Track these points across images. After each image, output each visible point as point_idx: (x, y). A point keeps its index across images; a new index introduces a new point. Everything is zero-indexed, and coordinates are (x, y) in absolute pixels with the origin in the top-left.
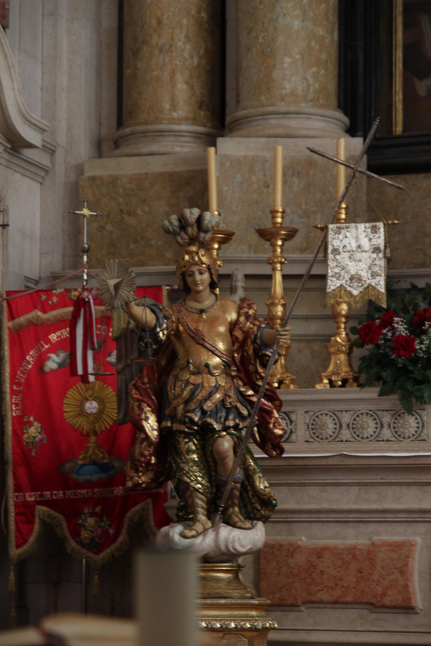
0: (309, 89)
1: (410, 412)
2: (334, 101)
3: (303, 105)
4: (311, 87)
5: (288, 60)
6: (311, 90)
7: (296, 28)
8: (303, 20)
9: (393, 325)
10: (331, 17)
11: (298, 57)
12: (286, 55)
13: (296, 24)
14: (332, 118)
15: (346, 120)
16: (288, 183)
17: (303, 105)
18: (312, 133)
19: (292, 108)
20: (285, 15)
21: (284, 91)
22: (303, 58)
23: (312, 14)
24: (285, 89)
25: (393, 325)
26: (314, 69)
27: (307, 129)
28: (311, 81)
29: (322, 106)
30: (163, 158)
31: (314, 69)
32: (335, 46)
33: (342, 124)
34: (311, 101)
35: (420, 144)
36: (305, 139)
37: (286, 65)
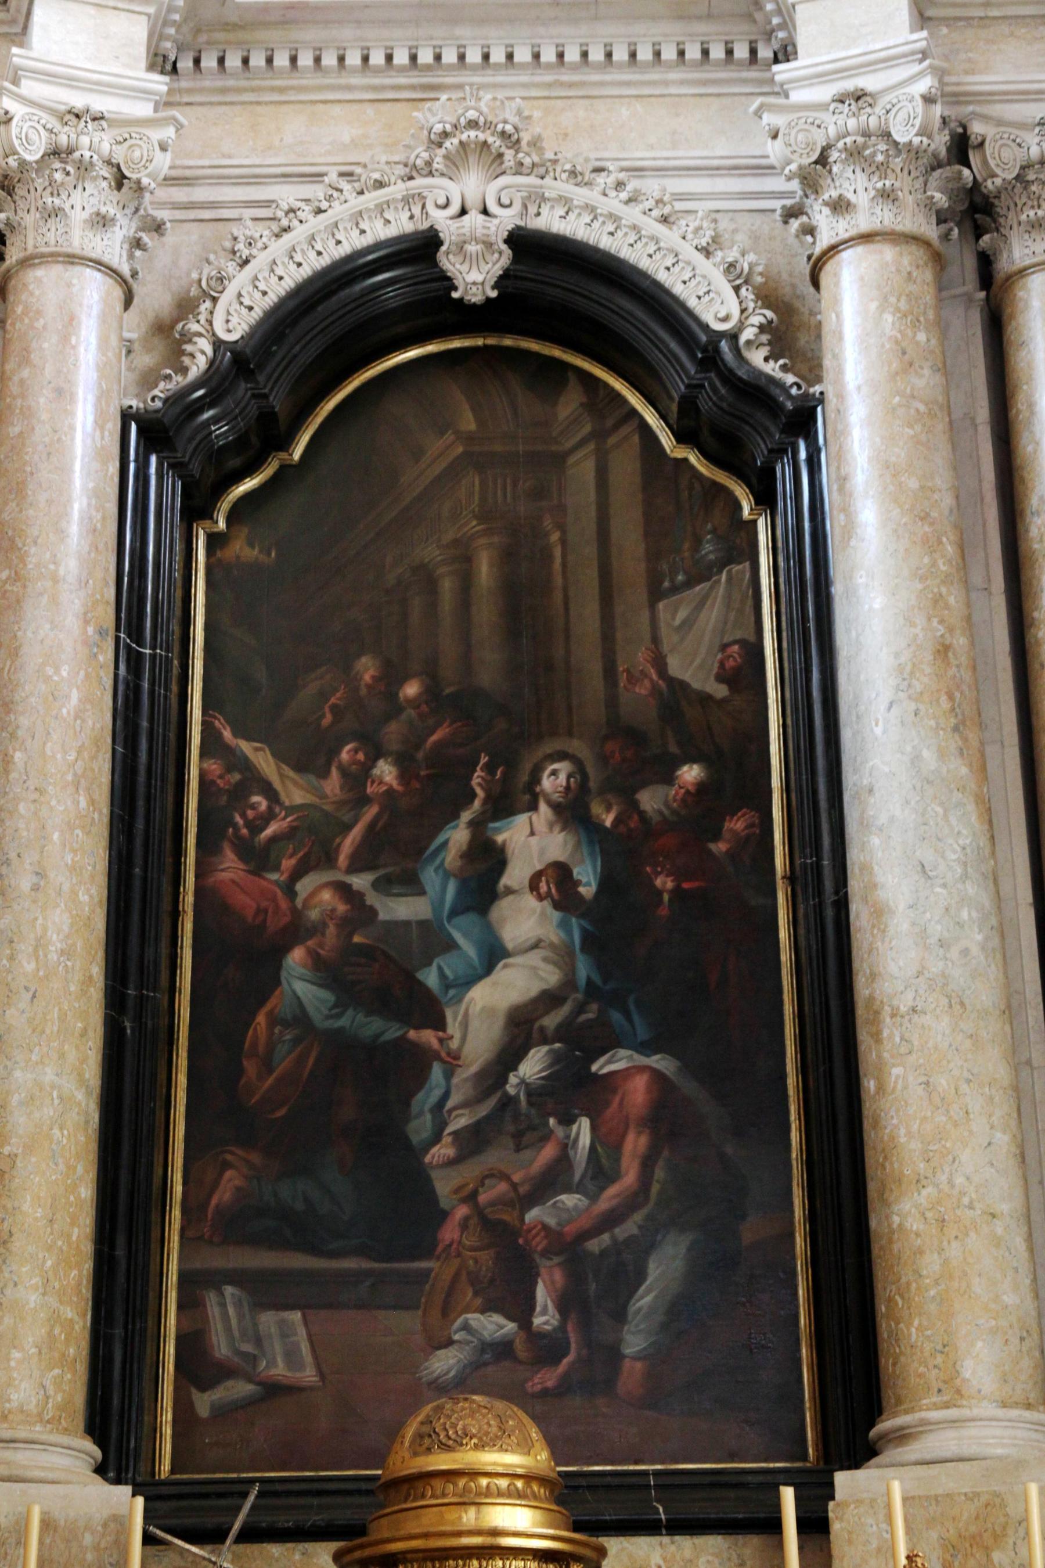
0: (47, 1403)
2: (80, 1423)
3: (38, 1428)
4: (51, 1400)
5: (16, 1355)
6: (50, 1405)
7: (32, 1305)
8: (44, 1294)
9: (395, 784)
10: (84, 1291)
11: (33, 1350)
12: (15, 1347)
13: (33, 1299)
14: (79, 1451)
15: (98, 1453)
16: (9, 1557)
17: (38, 1428)
18: (50, 1476)
19: (22, 1434)
20: (16, 1285)
21: (7, 1405)
22: (40, 1353)
23: (57, 1285)
24: (9, 1401)
25: (395, 784)
26: (57, 1371)
27: (43, 1468)
28: (51, 1392)
29: (66, 1431)
30: (983, 1463)
31: (57, 1371)
32: (86, 1335)
33: (92, 1461)
34: (48, 1422)
35: (206, 1496)
36: (40, 1485)
37: (13, 1364)
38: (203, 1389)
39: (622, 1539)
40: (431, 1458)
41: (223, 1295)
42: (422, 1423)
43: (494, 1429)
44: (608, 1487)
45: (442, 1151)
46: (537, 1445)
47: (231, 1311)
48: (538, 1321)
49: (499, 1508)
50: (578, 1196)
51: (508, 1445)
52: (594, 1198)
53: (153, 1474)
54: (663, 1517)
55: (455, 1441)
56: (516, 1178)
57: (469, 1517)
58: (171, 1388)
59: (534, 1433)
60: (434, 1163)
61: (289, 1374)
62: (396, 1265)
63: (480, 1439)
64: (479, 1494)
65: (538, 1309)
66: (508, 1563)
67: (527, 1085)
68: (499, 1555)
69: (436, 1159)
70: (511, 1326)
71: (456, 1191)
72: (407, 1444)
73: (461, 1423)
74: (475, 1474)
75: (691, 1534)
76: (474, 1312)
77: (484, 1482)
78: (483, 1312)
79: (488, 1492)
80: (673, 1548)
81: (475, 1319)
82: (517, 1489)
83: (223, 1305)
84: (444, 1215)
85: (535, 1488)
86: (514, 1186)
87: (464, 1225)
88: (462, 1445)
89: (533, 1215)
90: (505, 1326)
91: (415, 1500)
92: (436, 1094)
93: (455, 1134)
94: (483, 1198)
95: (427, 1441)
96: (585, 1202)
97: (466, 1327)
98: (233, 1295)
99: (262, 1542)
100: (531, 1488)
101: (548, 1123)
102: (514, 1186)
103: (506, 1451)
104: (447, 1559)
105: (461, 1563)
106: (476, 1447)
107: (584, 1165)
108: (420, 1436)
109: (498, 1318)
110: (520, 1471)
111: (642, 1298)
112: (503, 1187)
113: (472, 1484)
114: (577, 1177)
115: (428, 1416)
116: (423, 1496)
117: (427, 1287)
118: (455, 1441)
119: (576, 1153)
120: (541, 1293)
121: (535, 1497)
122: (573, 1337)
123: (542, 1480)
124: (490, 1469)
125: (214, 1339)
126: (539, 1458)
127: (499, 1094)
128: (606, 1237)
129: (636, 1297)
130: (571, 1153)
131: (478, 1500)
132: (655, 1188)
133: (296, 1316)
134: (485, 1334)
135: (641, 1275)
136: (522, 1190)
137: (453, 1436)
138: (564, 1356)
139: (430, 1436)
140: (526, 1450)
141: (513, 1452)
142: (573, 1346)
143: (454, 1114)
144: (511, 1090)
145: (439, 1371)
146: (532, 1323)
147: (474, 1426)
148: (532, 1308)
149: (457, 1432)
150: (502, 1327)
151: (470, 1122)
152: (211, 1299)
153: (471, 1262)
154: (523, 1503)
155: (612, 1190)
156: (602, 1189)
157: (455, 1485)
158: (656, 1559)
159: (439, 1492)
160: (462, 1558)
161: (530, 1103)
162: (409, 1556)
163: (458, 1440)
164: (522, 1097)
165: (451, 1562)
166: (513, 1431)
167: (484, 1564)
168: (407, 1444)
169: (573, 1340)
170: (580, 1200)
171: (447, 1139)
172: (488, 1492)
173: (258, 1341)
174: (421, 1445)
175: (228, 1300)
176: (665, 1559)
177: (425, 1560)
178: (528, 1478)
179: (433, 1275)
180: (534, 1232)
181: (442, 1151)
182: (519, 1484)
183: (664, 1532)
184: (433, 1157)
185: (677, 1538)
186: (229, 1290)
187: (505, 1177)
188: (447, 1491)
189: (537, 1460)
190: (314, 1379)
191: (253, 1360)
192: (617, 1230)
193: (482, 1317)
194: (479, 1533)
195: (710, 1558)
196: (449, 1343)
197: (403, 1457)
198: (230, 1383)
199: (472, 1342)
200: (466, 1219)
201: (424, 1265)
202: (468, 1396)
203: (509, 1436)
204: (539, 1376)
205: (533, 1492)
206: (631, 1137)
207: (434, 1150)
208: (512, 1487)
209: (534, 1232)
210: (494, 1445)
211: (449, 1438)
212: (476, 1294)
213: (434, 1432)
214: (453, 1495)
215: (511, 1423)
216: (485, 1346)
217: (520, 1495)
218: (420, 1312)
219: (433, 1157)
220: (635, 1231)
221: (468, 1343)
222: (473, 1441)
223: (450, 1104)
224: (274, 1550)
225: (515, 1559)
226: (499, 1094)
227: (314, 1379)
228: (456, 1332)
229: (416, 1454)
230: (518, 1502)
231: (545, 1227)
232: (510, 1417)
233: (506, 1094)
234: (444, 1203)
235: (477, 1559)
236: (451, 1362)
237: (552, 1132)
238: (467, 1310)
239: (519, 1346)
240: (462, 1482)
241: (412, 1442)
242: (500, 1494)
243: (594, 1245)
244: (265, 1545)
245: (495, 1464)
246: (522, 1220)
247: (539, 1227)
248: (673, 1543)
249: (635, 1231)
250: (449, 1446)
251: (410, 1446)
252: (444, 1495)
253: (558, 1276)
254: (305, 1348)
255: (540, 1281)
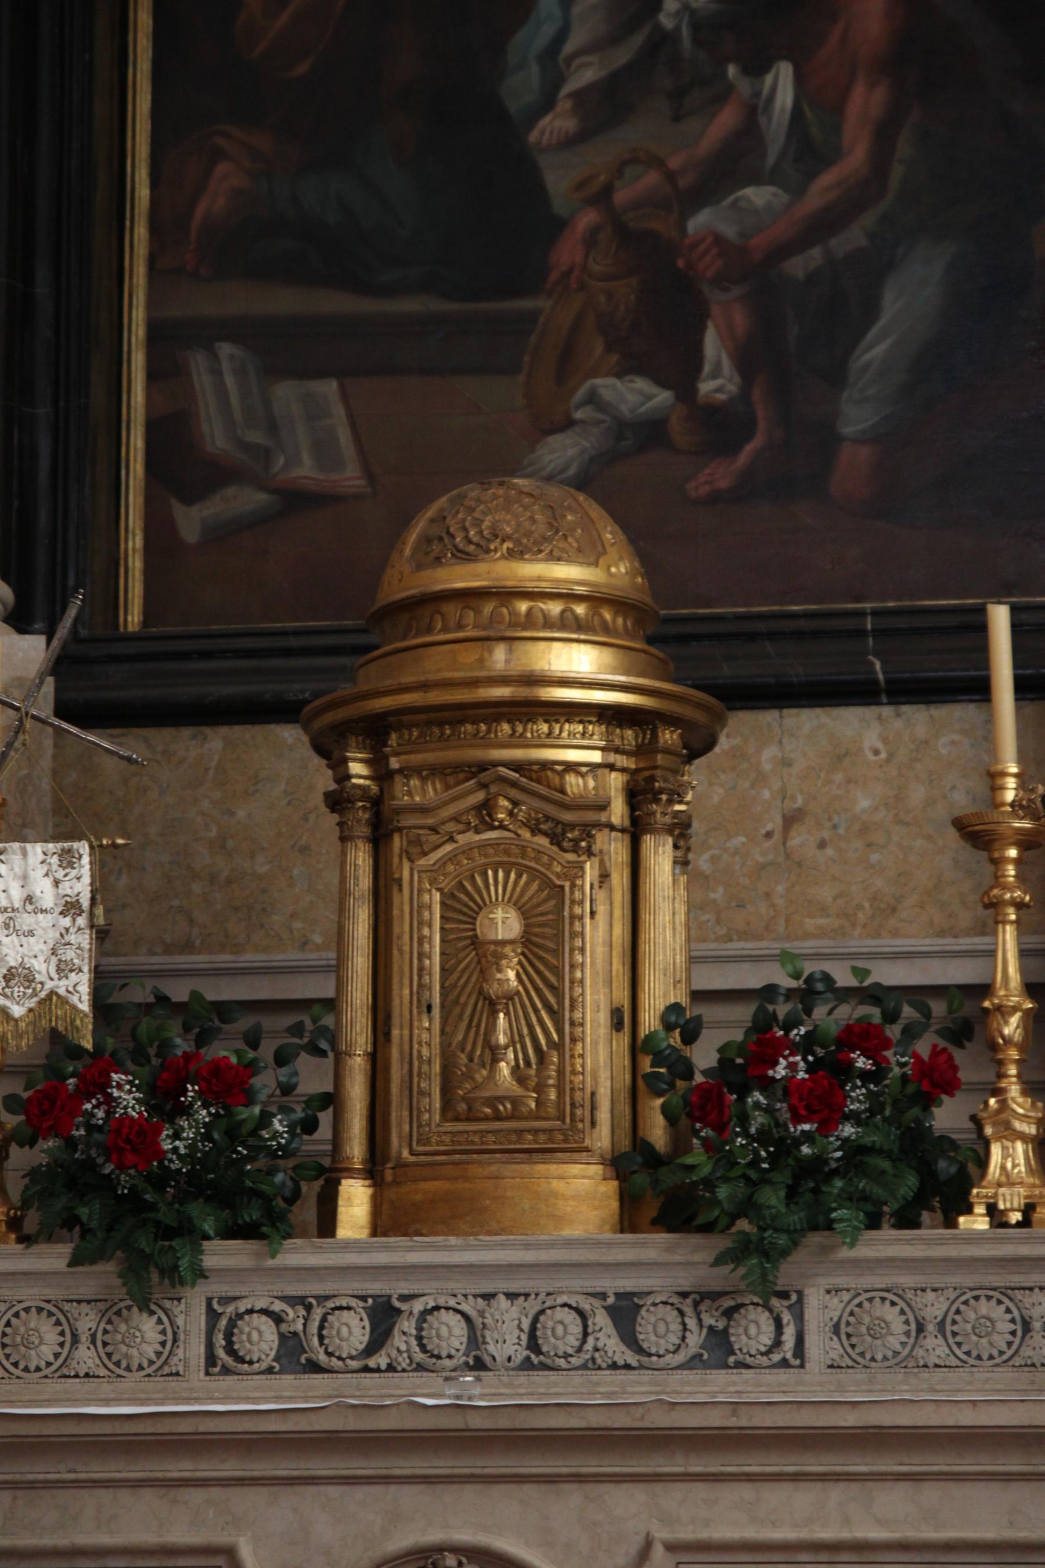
1: (145, 1306)
38: (189, 500)
39: (819, 711)
40: (441, 573)
41: (216, 357)
42: (432, 520)
43: (540, 527)
44: (799, 635)
45: (557, 124)
46: (613, 553)
47: (229, 380)
48: (706, 387)
49: (557, 645)
50: (772, 189)
51: (563, 550)
52: (798, 192)
53: (116, 626)
54: (881, 676)
55: (478, 545)
56: (674, 163)
57: (499, 657)
58: (141, 500)
59: (610, 534)
60: (544, 142)
61: (321, 477)
62: (485, 306)
63: (517, 542)
64: (514, 625)
65: (707, 368)
66: (557, 727)
67: (693, 12)
68: (542, 715)
69: (547, 136)
70: (663, 397)
71: (580, 186)
72: (408, 552)
73: (489, 518)
74: (508, 595)
75: (928, 703)
76: (607, 375)
77: (523, 606)
78: (619, 375)
79: (529, 621)
80: (898, 724)
81: (608, 387)
82: (576, 618)
83: (216, 372)
84: (559, 225)
85: (608, 616)
86: (671, 177)
87: (591, 240)
88: (488, 551)
89: (700, 221)
90: (655, 396)
91: (415, 636)
92: (547, 32)
93: (577, 96)
94: (620, 197)
95: (436, 547)
96: (784, 198)
97: (593, 399)
98: (231, 357)
99: (269, 722)
100: (600, 615)
101: (725, 73)
102: (671, 177)
103: (559, 559)
104: (462, 722)
105: (483, 727)
106: (511, 555)
107: (781, 139)
108: (427, 540)
109: (641, 384)
110: (580, 590)
111: (871, 347)
112: (652, 178)
113: (504, 610)
114: (771, 158)
115: (442, 509)
116: (429, 630)
117: (533, 339)
118: (478, 545)
119: (770, 119)
120: (712, 344)
121: (606, 629)
122: (762, 412)
123: (618, 604)
124: (530, 586)
125: (205, 428)
126: (613, 570)
127: (646, 30)
128: (816, 254)
129: (863, 345)
130: (762, 120)
131: (509, 634)
132: (897, 173)
133: (329, 388)
134: (624, 408)
135: (871, 311)
136: (683, 182)
137: (475, 539)
138: (749, 438)
139: (441, 539)
140: (592, 559)
141: (569, 561)
142: (762, 425)
143: (577, 62)
144: (666, 21)
145: (552, 465)
146: (695, 391)
147: (508, 523)
148: (698, 367)
149: (481, 532)
150: (650, 397)
151: (603, 73)
152: (198, 363)
153: (602, 298)
154: (582, 637)
155: (827, 179)
156: (811, 175)
157: (478, 612)
158: (872, 738)
159: (452, 624)
160: (484, 721)
161: (697, 42)
162: (406, 718)
163: (483, 543)
164: (685, 31)
165: (469, 727)
166: (572, 530)
167: (520, 728)
168: (408, 552)
169: (760, 414)
170: (775, 195)
171: (563, 105)
172: (529, 621)
173: (272, 427)
174: (427, 553)
175: (226, 366)
176: (885, 740)
177: (430, 723)
178: (594, 599)
179: (542, 319)
180: (702, 247)
181: (557, 124)
182: (580, 609)
183: (884, 700)
184: (542, 133)
185: (905, 709)
186: (225, 349)
187: (659, 163)
188: (464, 622)
189: (610, 574)
190: (358, 482)
191: (265, 455)
192: (833, 243)
193: (618, 384)
194: (504, 680)
195: (956, 737)
196: (569, 423)
197: (401, 573)
198: (230, 491)
199: (603, 422)
200: (594, 231)
201: (527, 304)
202: (505, 479)
203: (565, 536)
204: (707, 471)
205: (604, 622)
206: (858, 93)
207: (545, 121)
208: (568, 614)
209: (702, 247)
210: (540, 551)
211: (470, 542)
212: (609, 349)
213: (448, 533)
214: (474, 627)
215: (569, 518)
216: (621, 427)
217: (580, 625)
218: (521, 378)
219: (542, 133)
220: (863, 242)
221: (597, 423)
222: (505, 546)
223: (569, 47)
224: (286, 734)
225: (568, 721)
226: (646, 30)
227: (358, 482)
228: (577, 407)
229: (419, 567)
230: (574, 636)
231: (719, 240)
232: (570, 509)
233: (658, 27)
234: (560, 206)
235: (509, 722)
236: (571, 452)
237: (730, 88)
238: (594, 373)
239: (677, 428)
240: (488, 608)
241: (416, 548)
242: (548, 623)
243: (797, 267)
244: (272, 726)
245: (540, 579)
246: (683, 230)
247: (710, 240)
248: (898, 715)
249: (863, 242)
250: (468, 554)
251: (412, 555)
252: (460, 627)
253: (740, 319)
254: (344, 436)
255: (710, 325)
